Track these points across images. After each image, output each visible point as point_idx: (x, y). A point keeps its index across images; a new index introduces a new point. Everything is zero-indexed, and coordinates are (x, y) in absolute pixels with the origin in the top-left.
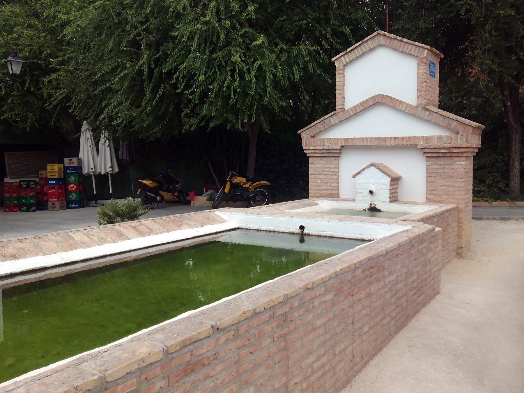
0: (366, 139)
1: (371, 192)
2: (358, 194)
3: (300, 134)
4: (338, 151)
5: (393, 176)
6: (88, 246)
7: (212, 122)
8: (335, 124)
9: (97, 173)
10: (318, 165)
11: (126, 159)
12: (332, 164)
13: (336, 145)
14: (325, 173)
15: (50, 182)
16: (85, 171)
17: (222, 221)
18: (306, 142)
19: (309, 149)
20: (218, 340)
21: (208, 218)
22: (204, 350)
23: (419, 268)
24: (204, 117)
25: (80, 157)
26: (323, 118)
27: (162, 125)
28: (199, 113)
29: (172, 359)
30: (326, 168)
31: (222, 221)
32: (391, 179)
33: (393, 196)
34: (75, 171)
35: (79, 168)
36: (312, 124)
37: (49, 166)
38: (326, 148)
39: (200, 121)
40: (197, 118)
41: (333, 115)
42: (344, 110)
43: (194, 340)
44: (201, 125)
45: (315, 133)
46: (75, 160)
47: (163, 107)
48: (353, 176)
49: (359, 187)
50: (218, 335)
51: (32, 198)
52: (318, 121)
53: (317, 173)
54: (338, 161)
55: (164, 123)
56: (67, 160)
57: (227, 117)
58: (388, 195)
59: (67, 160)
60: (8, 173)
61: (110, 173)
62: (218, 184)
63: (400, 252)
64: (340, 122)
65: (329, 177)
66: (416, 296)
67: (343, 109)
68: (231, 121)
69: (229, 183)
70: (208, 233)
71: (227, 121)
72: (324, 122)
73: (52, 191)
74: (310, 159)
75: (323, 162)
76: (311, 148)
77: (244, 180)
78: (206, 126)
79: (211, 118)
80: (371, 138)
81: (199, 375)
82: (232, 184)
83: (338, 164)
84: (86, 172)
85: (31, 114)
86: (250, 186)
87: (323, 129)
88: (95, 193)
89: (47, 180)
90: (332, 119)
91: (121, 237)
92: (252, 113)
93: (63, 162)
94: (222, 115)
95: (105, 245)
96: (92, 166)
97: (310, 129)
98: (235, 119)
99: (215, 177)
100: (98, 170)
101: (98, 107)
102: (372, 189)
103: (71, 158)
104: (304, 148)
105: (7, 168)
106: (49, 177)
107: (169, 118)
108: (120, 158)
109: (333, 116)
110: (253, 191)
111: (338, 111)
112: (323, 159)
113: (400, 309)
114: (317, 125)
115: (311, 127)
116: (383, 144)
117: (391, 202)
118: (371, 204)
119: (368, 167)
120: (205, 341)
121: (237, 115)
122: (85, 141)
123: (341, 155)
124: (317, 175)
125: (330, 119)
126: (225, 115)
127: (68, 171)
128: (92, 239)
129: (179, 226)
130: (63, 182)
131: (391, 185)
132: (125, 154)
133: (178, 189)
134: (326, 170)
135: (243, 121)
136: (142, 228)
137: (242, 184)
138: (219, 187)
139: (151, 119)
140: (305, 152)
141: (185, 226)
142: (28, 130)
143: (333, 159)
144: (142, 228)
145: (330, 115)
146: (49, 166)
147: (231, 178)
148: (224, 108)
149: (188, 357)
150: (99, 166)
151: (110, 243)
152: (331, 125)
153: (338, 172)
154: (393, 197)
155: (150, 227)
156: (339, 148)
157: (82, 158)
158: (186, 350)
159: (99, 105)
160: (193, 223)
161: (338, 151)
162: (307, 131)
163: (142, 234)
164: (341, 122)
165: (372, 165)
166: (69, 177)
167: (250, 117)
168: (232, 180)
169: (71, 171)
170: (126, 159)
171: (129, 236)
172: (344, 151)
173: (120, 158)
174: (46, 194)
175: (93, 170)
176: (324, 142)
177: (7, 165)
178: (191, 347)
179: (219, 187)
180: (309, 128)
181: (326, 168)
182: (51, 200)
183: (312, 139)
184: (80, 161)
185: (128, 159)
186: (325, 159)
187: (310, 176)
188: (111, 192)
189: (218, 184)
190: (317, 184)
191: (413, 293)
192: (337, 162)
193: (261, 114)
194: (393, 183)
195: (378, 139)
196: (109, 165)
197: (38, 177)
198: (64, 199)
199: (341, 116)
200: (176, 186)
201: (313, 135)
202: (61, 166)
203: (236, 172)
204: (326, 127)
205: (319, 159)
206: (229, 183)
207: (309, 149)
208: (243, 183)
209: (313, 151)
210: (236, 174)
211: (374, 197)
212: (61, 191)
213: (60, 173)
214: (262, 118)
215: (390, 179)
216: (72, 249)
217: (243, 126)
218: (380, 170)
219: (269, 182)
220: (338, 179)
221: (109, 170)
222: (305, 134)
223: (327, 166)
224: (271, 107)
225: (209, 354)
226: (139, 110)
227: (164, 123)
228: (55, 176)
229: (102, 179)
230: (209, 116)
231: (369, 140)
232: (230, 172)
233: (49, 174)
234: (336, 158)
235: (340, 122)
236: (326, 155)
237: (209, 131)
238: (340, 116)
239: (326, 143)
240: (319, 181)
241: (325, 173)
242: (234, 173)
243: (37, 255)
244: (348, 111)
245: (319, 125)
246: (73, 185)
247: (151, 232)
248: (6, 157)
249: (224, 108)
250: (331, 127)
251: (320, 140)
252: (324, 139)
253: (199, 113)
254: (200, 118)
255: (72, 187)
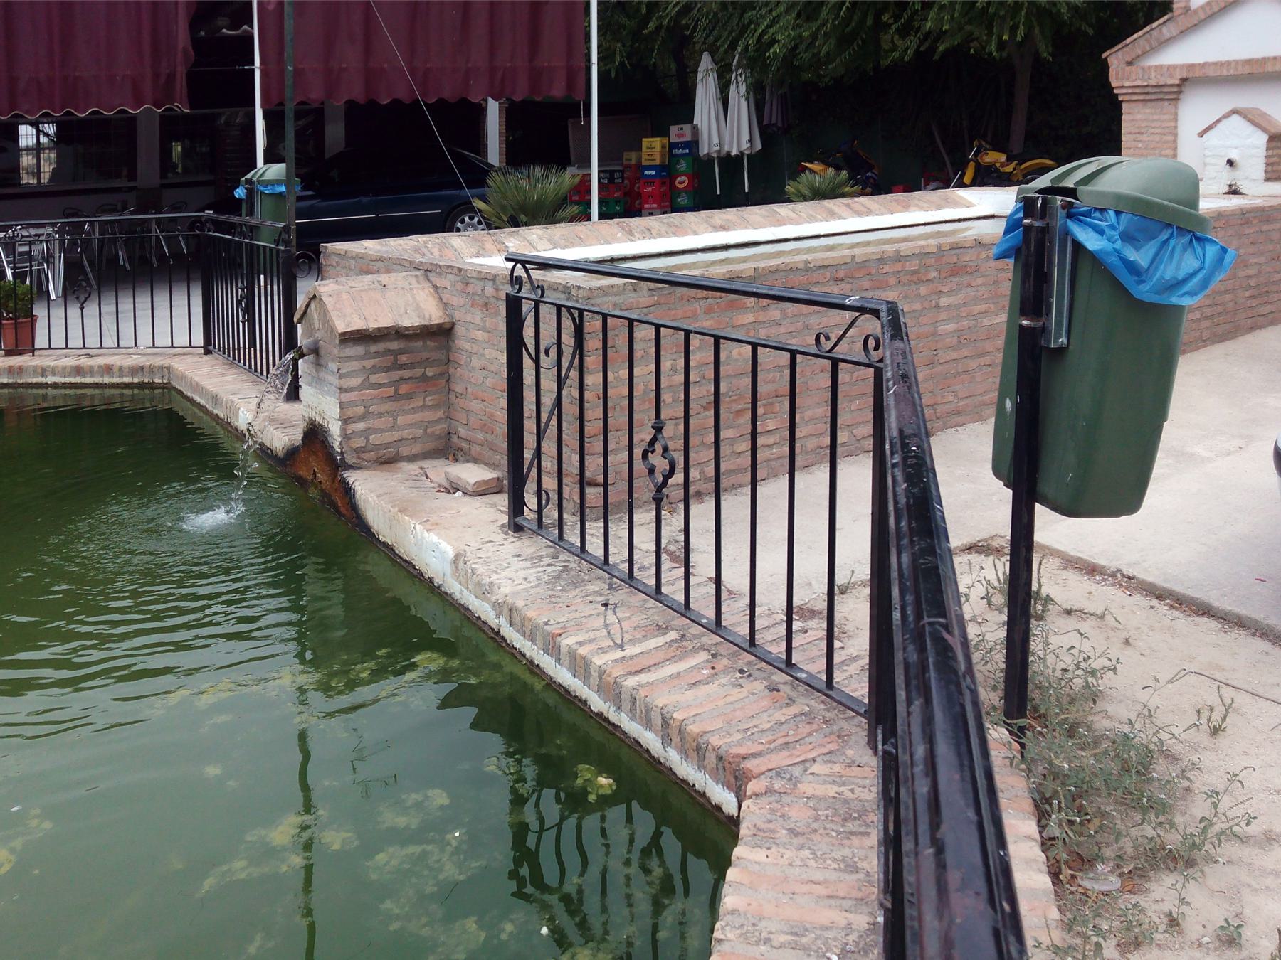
0: (1229, 63)
1: (1231, 163)
2: (1208, 168)
3: (1106, 58)
4: (1175, 89)
5: (1273, 131)
6: (797, 224)
7: (943, 42)
8: (1171, 38)
9: (723, 153)
10: (1139, 117)
11: (776, 124)
12: (1164, 114)
13: (1171, 76)
14: (1153, 131)
15: (646, 172)
16: (704, 150)
17: (969, 205)
18: (1117, 74)
19: (1122, 87)
20: (979, 253)
21: (946, 200)
22: (968, 257)
23: (1262, 259)
24: (929, 33)
25: (695, 123)
26: (1147, 29)
27: (850, 53)
28: (920, 27)
29: (943, 256)
30: (1153, 121)
31: (969, 205)
32: (1267, 137)
33: (1274, 169)
34: (687, 151)
35: (693, 144)
36: (1128, 40)
37: (645, 142)
38: (1153, 82)
39: (922, 42)
40: (916, 35)
41: (1168, 20)
42: (1187, 11)
43: (960, 246)
44: (922, 48)
45: (1134, 56)
46: (687, 128)
47: (855, 17)
48: (1199, 134)
49: (1210, 153)
50: (980, 250)
51: (617, 202)
52: (1140, 33)
53: (1137, 131)
54: (1176, 108)
55: (854, 49)
56: (674, 130)
57: (971, 34)
58: (1263, 167)
59: (674, 130)
60: (573, 159)
61: (746, 152)
62: (950, 170)
63: (1221, 224)
64: (1181, 33)
65: (1157, 138)
66: (1255, 302)
67: (1187, 9)
68: (978, 38)
69: (972, 165)
70: (947, 219)
71: (970, 38)
72: (1151, 35)
73: (649, 189)
74: (1124, 105)
75: (1148, 111)
76: (1127, 84)
77: (1002, 158)
78: (932, 49)
79: (941, 35)
80: (1237, 62)
81: (964, 279)
82: (978, 167)
83: (1176, 114)
84: (706, 152)
85: (619, 45)
86: (1014, 169)
87: (1148, 48)
88: (718, 193)
89: (640, 167)
90: (1165, 30)
91: (833, 215)
92: (1019, 22)
93: (666, 134)
94: (960, 29)
95: (816, 223)
96: (715, 140)
97: (1125, 49)
98: (986, 35)
99: (945, 156)
100: (726, 148)
101: (738, 24)
102: (1233, 155)
103: (680, 126)
104: (1113, 85)
105: (572, 149)
106: (644, 163)
107: (862, 39)
108: (765, 123)
109: (1167, 24)
110: (1021, 179)
111: (1176, 12)
112: (1149, 104)
113: (1220, 309)
114: (1138, 41)
115: (1126, 45)
116: (1261, 71)
117: (1267, 180)
118: (1230, 186)
119: (1226, 116)
120: (969, 250)
121: (990, 27)
122: (704, 94)
123: (1181, 96)
124: (1138, 135)
125: (1161, 28)
126: (968, 28)
127: (675, 151)
128: (800, 216)
129: (906, 207)
130: (667, 171)
131: (1268, 149)
132: (774, 114)
133: (871, 181)
134: (1153, 125)
135: (1000, 38)
136: (856, 206)
137: (998, 165)
138: (952, 176)
139: (833, 42)
140: (1116, 91)
141: (915, 208)
142: (613, 76)
143: (1166, 103)
144: (856, 206)
145: (1161, 21)
146: (645, 142)
147: (976, 155)
148: (967, 14)
149: (955, 259)
150: (727, 139)
151: (821, 221)
152: (1162, 40)
153: (1176, 127)
154: (1274, 171)
155: (868, 206)
156: (1177, 82)
157: (699, 126)
158: (954, 252)
159: (740, 20)
160: (925, 205)
161: (1175, 89)
162: (1120, 53)
163: (859, 214)
164: (1184, 33)
165: (1235, 112)
166: (678, 163)
167: (1014, 30)
168: (979, 158)
169: (681, 151)
170: (776, 124)
171: (844, 215)
172: (1187, 90)
173: (765, 123)
174: (639, 195)
175: (718, 148)
176: (1150, 74)
177: (571, 144)
178: (957, 251)
179: (952, 176)
180: (1122, 48)
181: (1153, 121)
182: (646, 206)
183: (1128, 69)
184: (695, 128)
185: (780, 124)
186: (1153, 104)
187: (1124, 138)
188: (747, 191)
189: (950, 170)
190: (1137, 151)
191: (1248, 294)
192: (1173, 110)
193: (1035, 23)
194: (1274, 144)
195: (1249, 62)
196: (746, 137)
197: (622, 164)
198: (667, 203)
199: (1183, 22)
200: (869, 174)
201: (1130, 60)
202: (665, 141)
203: (987, 142)
204: (1155, 44)
205: (1140, 104)
206: (972, 165)
207: (1122, 87)
208: (1001, 164)
209: (1130, 91)
210: (988, 147)
211: (1238, 173)
212: (663, 189)
213: (663, 155)
214: (1037, 30)
215: (1265, 137)
216: (780, 225)
217: (1001, 45)
218: (1250, 121)
219: (1053, 160)
220: (1175, 141)
221: (745, 146)
222: (1116, 59)
223: (1155, 117)
224: (1054, 10)
225: (970, 263)
226: (814, 26)
227: (854, 49)
228: (655, 160)
229: (731, 163)
230: (938, 31)
231: (1233, 65)
232: (976, 143)
233: (644, 157)
234: (1174, 102)
235: (1181, 33)
236: (1153, 97)
237: (936, 57)
238: (1180, 23)
239: (1153, 74)
240: (1140, 145)
241: (1153, 131)
242: (983, 143)
243: (746, 228)
244: (1196, 12)
245: (1142, 42)
246: (683, 178)
247: (869, 212)
248: (570, 126)
249: (967, 14)
250: (1162, 43)
251: (1143, 69)
252: (1149, 68)
253: (920, 27)
254: (922, 37)
255: (682, 181)
